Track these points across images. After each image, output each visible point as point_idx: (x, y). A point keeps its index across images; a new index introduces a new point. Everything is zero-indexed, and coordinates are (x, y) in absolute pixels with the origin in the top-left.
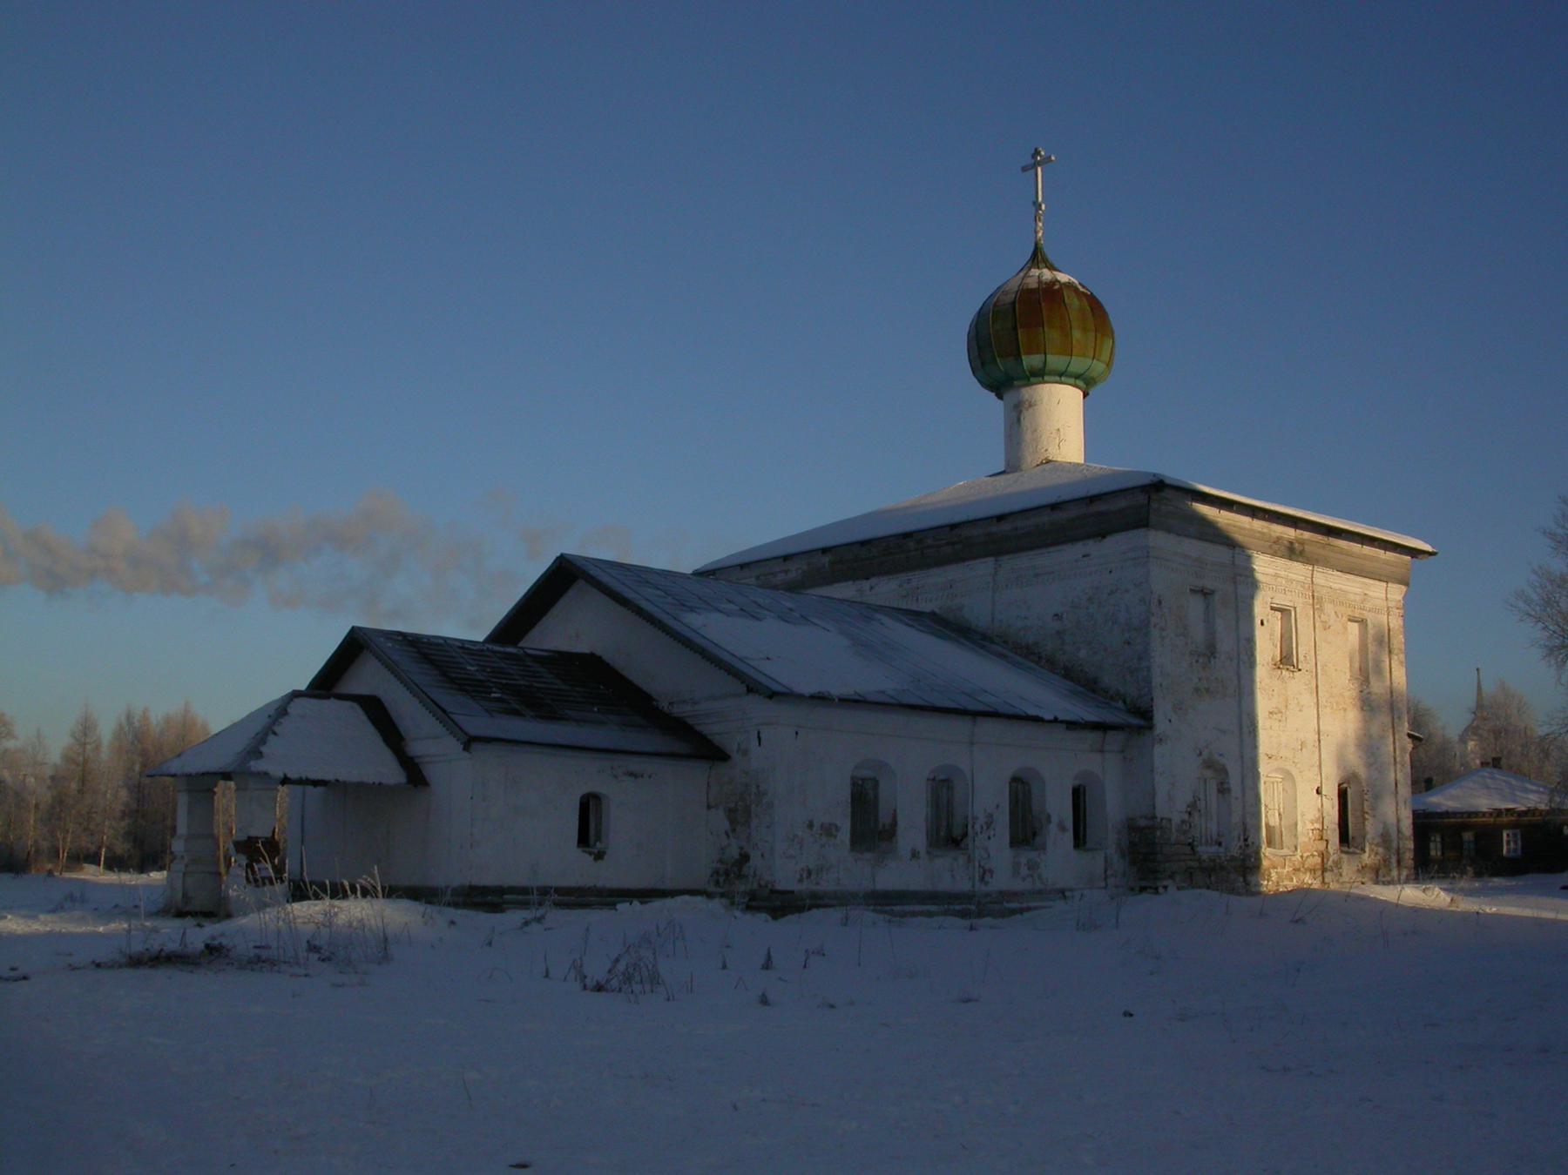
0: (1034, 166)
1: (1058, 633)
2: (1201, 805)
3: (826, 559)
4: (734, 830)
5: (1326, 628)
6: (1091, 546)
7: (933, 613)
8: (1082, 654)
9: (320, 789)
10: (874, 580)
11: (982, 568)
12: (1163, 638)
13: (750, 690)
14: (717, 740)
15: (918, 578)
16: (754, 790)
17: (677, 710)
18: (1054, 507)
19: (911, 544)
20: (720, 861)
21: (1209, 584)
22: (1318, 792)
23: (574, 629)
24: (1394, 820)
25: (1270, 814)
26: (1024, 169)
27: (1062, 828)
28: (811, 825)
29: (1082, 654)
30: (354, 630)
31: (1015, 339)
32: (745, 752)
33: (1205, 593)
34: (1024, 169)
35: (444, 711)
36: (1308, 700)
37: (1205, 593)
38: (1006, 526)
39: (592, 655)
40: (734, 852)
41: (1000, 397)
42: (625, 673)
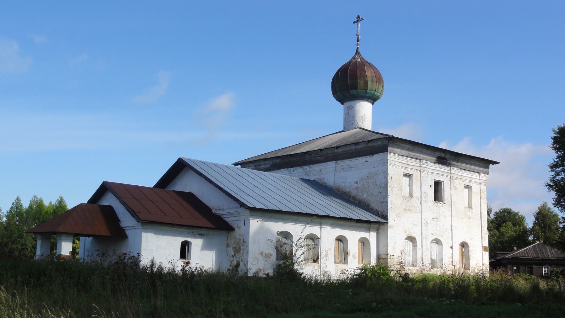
0: (358, 21)
1: (356, 188)
2: (406, 251)
3: (278, 161)
4: (235, 255)
5: (455, 188)
6: (368, 158)
7: (314, 180)
8: (365, 196)
9: (91, 238)
10: (294, 168)
11: (331, 165)
12: (392, 191)
13: (241, 206)
14: (230, 223)
15: (309, 168)
16: (242, 240)
17: (218, 213)
18: (356, 144)
19: (307, 156)
20: (230, 266)
21: (410, 172)
22: (451, 248)
23: (186, 184)
24: (298, 256)
25: (390, 252)
26: (354, 23)
27: (354, 257)
28: (262, 253)
29: (365, 196)
30: (104, 183)
31: (351, 84)
32: (239, 228)
33: (408, 176)
34: (354, 23)
35: (133, 211)
36: (448, 214)
37: (408, 176)
38: (339, 150)
39: (190, 193)
40: (235, 263)
41: (342, 104)
42: (201, 199)
